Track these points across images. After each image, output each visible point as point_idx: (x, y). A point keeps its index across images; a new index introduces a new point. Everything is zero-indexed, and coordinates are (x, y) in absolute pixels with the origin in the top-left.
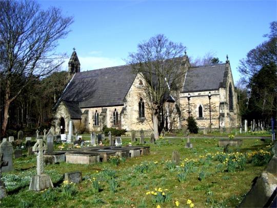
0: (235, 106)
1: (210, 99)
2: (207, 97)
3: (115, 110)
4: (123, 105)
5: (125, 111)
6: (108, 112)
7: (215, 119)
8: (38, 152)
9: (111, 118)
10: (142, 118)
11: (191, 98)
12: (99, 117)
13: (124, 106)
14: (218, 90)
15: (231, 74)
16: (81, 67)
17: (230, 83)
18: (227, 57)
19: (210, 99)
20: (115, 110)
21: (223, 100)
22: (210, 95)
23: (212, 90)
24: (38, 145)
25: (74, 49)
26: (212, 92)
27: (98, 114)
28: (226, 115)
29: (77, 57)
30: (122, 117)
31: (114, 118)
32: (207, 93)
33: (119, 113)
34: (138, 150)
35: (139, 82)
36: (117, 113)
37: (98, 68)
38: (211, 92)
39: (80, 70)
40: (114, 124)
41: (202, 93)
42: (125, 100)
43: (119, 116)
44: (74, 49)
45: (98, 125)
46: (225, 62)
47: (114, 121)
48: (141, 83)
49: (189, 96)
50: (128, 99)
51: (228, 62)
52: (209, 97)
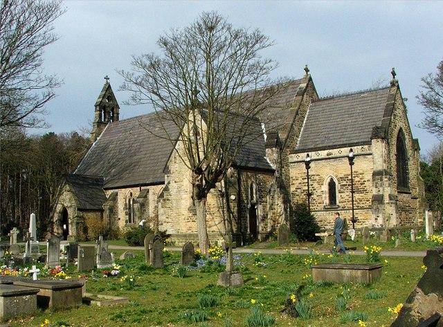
1: (352, 164)
2: (347, 160)
7: (362, 208)
11: (355, 160)
14: (369, 143)
17: (401, 130)
18: (394, 74)
19: (352, 164)
21: (380, 165)
23: (357, 144)
26: (357, 150)
28: (386, 200)
32: (345, 151)
38: (310, 153)
41: (335, 152)
42: (166, 170)
49: (308, 159)
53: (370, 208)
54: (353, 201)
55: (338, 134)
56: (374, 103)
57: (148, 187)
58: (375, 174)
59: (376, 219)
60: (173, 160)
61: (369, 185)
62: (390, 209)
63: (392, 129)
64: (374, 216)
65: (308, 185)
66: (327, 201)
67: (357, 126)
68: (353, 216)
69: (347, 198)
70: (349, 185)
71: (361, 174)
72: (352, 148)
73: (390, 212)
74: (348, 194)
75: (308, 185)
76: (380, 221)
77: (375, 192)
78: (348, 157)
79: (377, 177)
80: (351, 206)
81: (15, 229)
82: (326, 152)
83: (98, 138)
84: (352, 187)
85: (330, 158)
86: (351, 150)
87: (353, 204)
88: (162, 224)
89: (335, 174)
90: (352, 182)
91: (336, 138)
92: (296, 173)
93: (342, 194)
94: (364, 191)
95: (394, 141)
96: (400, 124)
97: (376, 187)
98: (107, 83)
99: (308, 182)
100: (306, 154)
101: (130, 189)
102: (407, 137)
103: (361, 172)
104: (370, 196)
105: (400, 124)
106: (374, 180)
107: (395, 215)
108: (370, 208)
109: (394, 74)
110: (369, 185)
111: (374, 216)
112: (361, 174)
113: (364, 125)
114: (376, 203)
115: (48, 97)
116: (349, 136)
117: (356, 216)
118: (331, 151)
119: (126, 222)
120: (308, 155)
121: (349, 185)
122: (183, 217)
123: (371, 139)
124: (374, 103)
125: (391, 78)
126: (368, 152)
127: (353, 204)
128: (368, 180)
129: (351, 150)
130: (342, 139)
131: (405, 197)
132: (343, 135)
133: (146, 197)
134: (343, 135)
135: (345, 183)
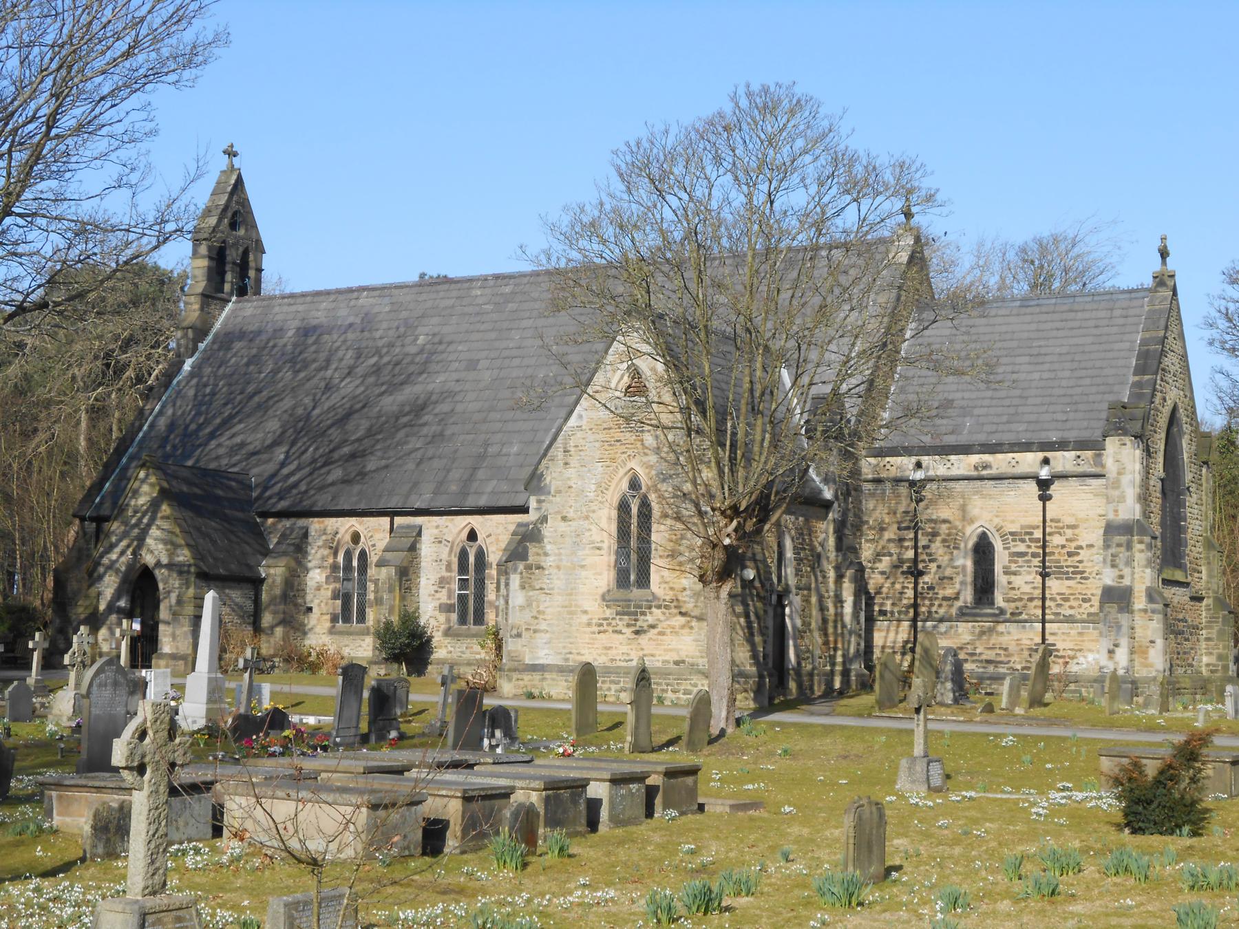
0: (1194, 548)
1: (1045, 498)
2: (1032, 488)
3: (472, 536)
4: (524, 510)
5: (532, 549)
6: (427, 549)
7: (1070, 620)
8: (141, 769)
9: (442, 582)
10: (636, 593)
11: (1056, 489)
12: (372, 572)
13: (532, 516)
14: (1096, 446)
15: (1184, 357)
16: (268, 262)
17: (1175, 409)
18: (1164, 254)
19: (1045, 498)
20: (472, 536)
21: (1130, 509)
22: (1044, 473)
23: (1062, 446)
24: (143, 735)
25: (231, 153)
26: (1064, 460)
27: (363, 555)
28: (1140, 602)
29: (245, 203)
30: (515, 580)
31: (463, 584)
32: (1029, 461)
33: (494, 556)
34: (634, 787)
35: (626, 380)
36: (481, 555)
37: (334, 287)
38: (925, 460)
39: (258, 281)
40: (463, 620)
41: (1000, 462)
42: (534, 482)
43: (492, 572)
44: (231, 153)
45: (362, 618)
46: (1149, 282)
47: (462, 599)
48: (636, 388)
49: (919, 475)
50: (554, 475)
51: (1164, 281)
52: (1044, 485)
53: (1092, 619)
54: (1044, 599)
55: (999, 410)
56: (1106, 330)
57: (419, 520)
58: (1111, 529)
59: (1111, 652)
60: (560, 455)
61: (1092, 560)
62: (1150, 628)
63: (1157, 410)
64: (1105, 644)
65: (916, 547)
66: (968, 596)
67: (1057, 392)
68: (1044, 639)
69: (1027, 589)
70: (1034, 555)
71: (1069, 527)
72: (1049, 454)
73: (1150, 634)
74: (1029, 578)
76: (1122, 656)
77: (1109, 577)
79: (1118, 539)
80: (1039, 612)
81: (82, 628)
82: (975, 459)
83: (202, 346)
84: (1044, 561)
85: (981, 478)
86: (1046, 461)
87: (1044, 608)
88: (519, 635)
89: (996, 521)
93: (1013, 578)
95: (1160, 445)
96: (1173, 394)
97: (1113, 566)
98: (232, 168)
99: (916, 539)
100: (914, 459)
102: (1186, 428)
103: (1069, 520)
104: (1094, 588)
105: (1173, 394)
106: (1107, 546)
107: (1160, 642)
108: (1092, 619)
110: (1092, 560)
112: (1069, 527)
113: (1079, 390)
114: (1112, 609)
116: (1033, 417)
118: (987, 458)
119: (334, 619)
120: (919, 465)
121: (1034, 555)
122: (585, 618)
124: (1106, 330)
126: (1093, 470)
127: (1044, 608)
128: (1091, 546)
129: (1046, 461)
131: (1178, 596)
133: (413, 548)
134: (1017, 414)
135: (1021, 548)
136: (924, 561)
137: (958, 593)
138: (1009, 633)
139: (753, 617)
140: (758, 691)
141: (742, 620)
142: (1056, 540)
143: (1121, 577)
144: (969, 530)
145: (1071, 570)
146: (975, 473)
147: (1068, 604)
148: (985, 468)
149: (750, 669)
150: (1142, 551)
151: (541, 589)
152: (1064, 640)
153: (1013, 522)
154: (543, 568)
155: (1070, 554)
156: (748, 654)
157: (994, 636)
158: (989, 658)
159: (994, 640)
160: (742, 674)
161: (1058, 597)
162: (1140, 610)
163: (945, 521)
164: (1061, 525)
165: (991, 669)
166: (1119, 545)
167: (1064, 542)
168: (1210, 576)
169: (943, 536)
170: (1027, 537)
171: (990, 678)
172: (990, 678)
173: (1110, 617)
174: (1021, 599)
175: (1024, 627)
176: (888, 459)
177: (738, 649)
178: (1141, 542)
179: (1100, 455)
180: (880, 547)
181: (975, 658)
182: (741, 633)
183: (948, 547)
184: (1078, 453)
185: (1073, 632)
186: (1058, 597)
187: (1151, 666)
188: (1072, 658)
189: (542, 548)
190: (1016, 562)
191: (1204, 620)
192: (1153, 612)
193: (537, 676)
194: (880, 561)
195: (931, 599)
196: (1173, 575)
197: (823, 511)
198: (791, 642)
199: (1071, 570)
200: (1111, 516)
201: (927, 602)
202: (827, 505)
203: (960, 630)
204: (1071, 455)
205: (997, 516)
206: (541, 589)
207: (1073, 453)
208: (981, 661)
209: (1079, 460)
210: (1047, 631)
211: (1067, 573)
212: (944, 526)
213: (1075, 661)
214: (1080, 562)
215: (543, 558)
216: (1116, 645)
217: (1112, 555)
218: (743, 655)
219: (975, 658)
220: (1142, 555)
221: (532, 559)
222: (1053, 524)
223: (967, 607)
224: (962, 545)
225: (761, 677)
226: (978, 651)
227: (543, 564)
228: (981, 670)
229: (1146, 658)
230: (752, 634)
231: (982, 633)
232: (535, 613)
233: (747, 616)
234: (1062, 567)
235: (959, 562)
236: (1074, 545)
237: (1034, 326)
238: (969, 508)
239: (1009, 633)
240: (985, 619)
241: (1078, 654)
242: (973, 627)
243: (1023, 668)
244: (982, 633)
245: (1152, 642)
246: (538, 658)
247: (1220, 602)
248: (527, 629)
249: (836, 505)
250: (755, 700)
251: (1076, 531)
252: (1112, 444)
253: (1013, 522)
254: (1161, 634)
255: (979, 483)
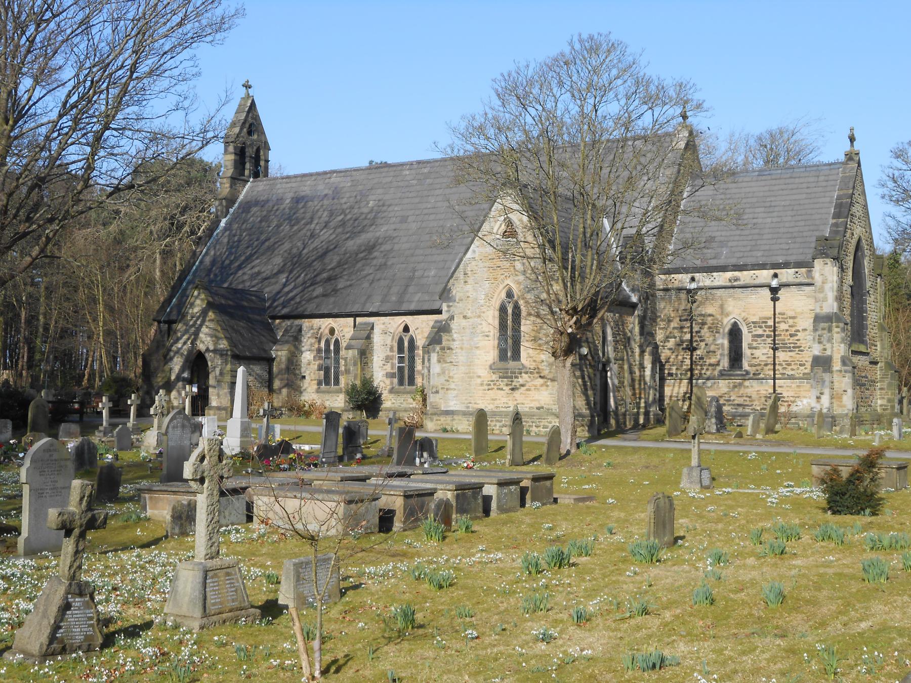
1: (775, 299)
2: (766, 293)
7: (791, 377)
11: (782, 294)
17: (859, 240)
18: (852, 139)
19: (775, 299)
21: (830, 306)
23: (786, 265)
26: (787, 275)
28: (837, 365)
32: (765, 275)
41: (745, 276)
42: (445, 294)
49: (693, 286)
52: (774, 291)
53: (806, 377)
54: (774, 364)
55: (745, 243)
60: (462, 276)
61: (806, 339)
62: (844, 382)
63: (848, 241)
64: (814, 393)
65: (691, 332)
66: (725, 363)
67: (782, 230)
69: (764, 358)
70: (768, 336)
71: (791, 318)
74: (765, 351)
75: (691, 332)
76: (825, 400)
77: (817, 350)
78: (769, 286)
79: (822, 325)
80: (772, 373)
82: (729, 275)
83: (231, 210)
84: (774, 340)
85: (733, 287)
86: (776, 276)
87: (774, 370)
88: (437, 392)
90: (774, 331)
91: (743, 249)
92: (662, 305)
93: (754, 351)
94: (797, 348)
96: (858, 231)
97: (820, 343)
98: (248, 96)
100: (690, 276)
101: (330, 320)
104: (807, 357)
106: (815, 330)
107: (850, 391)
108: (806, 377)
109: (852, 139)
110: (806, 339)
111: (814, 393)
112: (791, 318)
113: (796, 229)
114: (819, 370)
115: (808, 169)
116: (767, 247)
117: (779, 390)
118: (737, 274)
119: (319, 383)
120: (693, 279)
121: (768, 336)
122: (479, 381)
123: (814, 259)
125: (847, 147)
127: (774, 370)
128: (805, 330)
130: (754, 253)
132: (756, 245)
133: (368, 337)
134: (756, 245)
135: (760, 332)
136: (696, 341)
137: (719, 361)
138: (752, 387)
139: (587, 379)
140: (591, 425)
141: (580, 380)
142: (782, 327)
143: (825, 350)
144: (725, 321)
145: (792, 345)
146: (729, 284)
147: (790, 367)
148: (736, 280)
149: (585, 411)
150: (838, 333)
151: (451, 362)
152: (788, 391)
153: (754, 315)
154: (452, 349)
155: (791, 335)
156: (584, 402)
157: (743, 389)
158: (739, 403)
159: (742, 391)
160: (580, 415)
161: (784, 363)
162: (837, 371)
163: (710, 315)
164: (785, 316)
165: (740, 410)
166: (823, 329)
167: (788, 328)
168: (883, 348)
169: (709, 325)
170: (763, 325)
171: (740, 416)
172: (740, 416)
173: (818, 375)
174: (760, 365)
175: (762, 383)
176: (673, 276)
177: (577, 399)
178: (837, 327)
179: (811, 271)
180: (668, 332)
181: (730, 403)
182: (579, 389)
183: (712, 332)
184: (797, 270)
185: (794, 385)
186: (784, 363)
187: (844, 406)
188: (793, 402)
189: (451, 336)
190: (756, 341)
191: (878, 377)
192: (846, 372)
193: (449, 418)
194: (669, 341)
195: (701, 365)
196: (859, 348)
197: (632, 309)
198: (611, 394)
199: (792, 345)
200: (818, 311)
201: (699, 367)
202: (634, 306)
203: (720, 385)
204: (791, 271)
205: (744, 311)
206: (451, 362)
207: (793, 270)
208: (734, 405)
209: (797, 275)
210: (777, 385)
211: (790, 347)
212: (710, 319)
213: (795, 404)
214: (798, 340)
215: (452, 343)
216: (822, 394)
217: (819, 336)
218: (581, 403)
219: (730, 403)
220: (839, 335)
221: (444, 343)
222: (780, 316)
223: (725, 370)
224: (721, 330)
225: (592, 416)
226: (732, 398)
227: (452, 346)
228: (734, 410)
229: (841, 402)
230: (586, 390)
231: (735, 387)
232: (447, 378)
233: (583, 378)
234: (786, 344)
235: (719, 341)
236: (794, 329)
237: (767, 188)
238: (726, 306)
239: (752, 387)
240: (737, 378)
241: (797, 399)
242: (729, 383)
243: (761, 409)
244: (735, 387)
245: (845, 391)
246: (450, 406)
247: (889, 365)
248: (442, 388)
249: (639, 306)
250: (589, 431)
251: (795, 320)
252: (818, 264)
253: (754, 315)
254: (850, 386)
255: (732, 290)
